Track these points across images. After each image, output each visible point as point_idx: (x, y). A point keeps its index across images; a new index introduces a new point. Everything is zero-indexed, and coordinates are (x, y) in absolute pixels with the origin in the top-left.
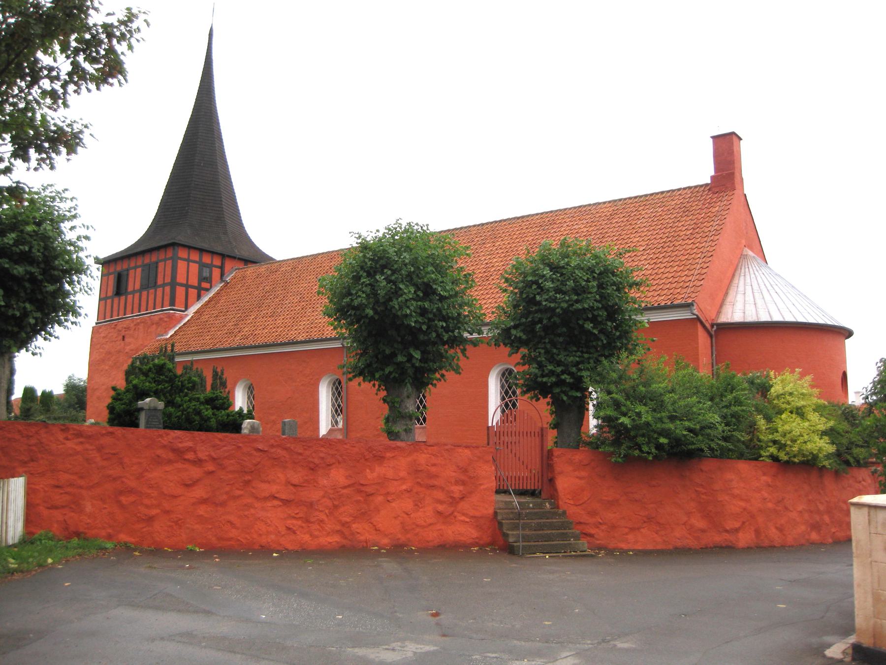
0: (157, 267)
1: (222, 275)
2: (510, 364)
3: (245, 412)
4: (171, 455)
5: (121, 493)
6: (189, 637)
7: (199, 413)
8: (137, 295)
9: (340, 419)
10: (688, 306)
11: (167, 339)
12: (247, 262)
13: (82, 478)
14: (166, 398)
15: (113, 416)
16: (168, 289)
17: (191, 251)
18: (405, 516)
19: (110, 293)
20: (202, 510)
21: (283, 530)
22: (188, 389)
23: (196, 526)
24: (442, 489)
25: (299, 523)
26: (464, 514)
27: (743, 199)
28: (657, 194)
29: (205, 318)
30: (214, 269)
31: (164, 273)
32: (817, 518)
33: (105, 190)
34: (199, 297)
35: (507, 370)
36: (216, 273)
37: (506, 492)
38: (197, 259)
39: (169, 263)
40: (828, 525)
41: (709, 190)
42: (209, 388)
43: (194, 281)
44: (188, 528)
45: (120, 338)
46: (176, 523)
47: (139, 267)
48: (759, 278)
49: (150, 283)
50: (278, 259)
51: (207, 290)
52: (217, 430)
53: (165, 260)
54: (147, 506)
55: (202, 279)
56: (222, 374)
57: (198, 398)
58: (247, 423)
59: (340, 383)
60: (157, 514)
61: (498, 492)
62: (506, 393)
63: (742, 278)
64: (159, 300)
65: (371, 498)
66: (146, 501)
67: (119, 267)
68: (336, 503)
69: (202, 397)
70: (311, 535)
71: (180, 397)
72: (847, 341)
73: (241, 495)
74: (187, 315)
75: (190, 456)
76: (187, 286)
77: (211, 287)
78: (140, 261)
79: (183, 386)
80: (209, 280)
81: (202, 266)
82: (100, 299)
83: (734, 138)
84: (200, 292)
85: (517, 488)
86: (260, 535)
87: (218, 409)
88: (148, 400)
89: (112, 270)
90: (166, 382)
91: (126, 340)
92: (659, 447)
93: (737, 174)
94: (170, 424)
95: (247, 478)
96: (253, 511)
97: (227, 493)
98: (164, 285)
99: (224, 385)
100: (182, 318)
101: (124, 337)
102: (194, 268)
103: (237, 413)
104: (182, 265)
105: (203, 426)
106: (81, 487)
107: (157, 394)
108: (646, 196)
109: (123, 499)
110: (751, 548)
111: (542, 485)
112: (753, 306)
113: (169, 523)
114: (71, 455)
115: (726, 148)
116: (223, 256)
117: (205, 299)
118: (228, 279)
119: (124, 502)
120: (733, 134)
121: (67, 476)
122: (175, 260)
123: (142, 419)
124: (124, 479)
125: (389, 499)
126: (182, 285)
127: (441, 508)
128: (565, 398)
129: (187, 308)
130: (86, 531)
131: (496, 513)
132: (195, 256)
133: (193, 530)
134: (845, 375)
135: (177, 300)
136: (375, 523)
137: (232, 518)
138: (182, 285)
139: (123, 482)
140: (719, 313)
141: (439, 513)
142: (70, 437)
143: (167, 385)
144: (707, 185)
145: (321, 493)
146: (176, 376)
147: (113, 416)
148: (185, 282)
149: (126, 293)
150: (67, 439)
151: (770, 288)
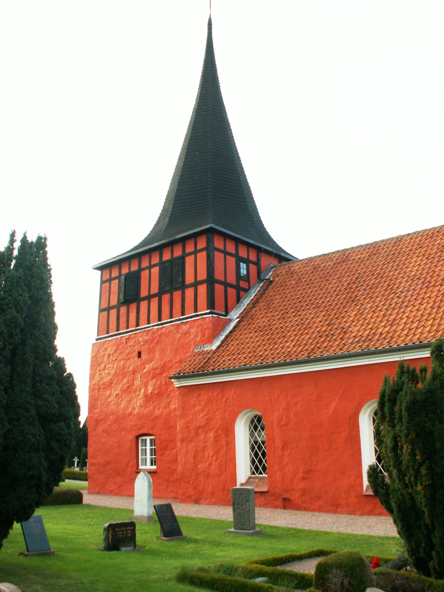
8: (154, 303)
16: (202, 290)
19: (114, 301)
34: (238, 300)
35: (255, 417)
39: (202, 257)
43: (232, 279)
45: (136, 353)
50: (300, 258)
51: (246, 291)
74: (230, 321)
76: (226, 285)
82: (101, 310)
89: (115, 273)
98: (149, 298)
102: (231, 261)
110: (57, 577)
116: (259, 250)
117: (246, 302)
126: (220, 283)
138: (220, 283)
149: (183, 286)
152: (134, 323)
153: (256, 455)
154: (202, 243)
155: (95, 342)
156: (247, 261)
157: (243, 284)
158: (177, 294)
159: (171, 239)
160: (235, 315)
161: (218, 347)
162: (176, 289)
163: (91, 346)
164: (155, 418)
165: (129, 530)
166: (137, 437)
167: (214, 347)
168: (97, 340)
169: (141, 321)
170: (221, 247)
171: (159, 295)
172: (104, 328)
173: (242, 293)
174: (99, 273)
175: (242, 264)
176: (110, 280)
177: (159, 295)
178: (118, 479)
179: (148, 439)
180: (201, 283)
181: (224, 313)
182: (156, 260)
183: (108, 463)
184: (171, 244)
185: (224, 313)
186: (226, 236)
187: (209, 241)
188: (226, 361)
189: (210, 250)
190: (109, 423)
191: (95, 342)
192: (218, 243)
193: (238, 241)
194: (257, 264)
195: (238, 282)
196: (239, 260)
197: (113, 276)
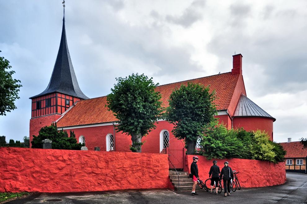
0: (51, 100)
1: (73, 103)
2: (167, 130)
3: (82, 144)
4: (53, 159)
5: (33, 173)
6: (76, 197)
7: (65, 144)
9: (112, 148)
10: (226, 110)
13: (17, 167)
14: (53, 139)
15: (33, 146)
16: (55, 107)
17: (62, 95)
18: (139, 178)
19: (35, 109)
20: (66, 178)
21: (96, 184)
22: (61, 136)
23: (64, 184)
24: (151, 168)
25: (102, 181)
26: (159, 177)
27: (242, 77)
29: (67, 116)
31: (53, 103)
32: (269, 178)
33: (33, 75)
34: (66, 110)
37: (174, 170)
39: (55, 98)
40: (272, 180)
41: (231, 74)
42: (69, 136)
43: (64, 105)
44: (61, 185)
46: (56, 183)
47: (44, 100)
48: (247, 103)
49: (49, 105)
51: (68, 108)
52: (72, 149)
53: (53, 97)
54: (44, 177)
55: (66, 104)
56: (74, 133)
57: (65, 139)
58: (82, 148)
59: (112, 136)
60: (49, 180)
61: (170, 169)
62: (165, 139)
63: (241, 102)
64: (47, 112)
65: (127, 172)
66: (44, 176)
67: (38, 100)
68: (115, 174)
69: (66, 139)
70: (107, 186)
71: (58, 139)
72: (274, 123)
73: (81, 172)
74: (62, 115)
75: (61, 158)
76: (61, 106)
78: (44, 98)
79: (59, 135)
81: (66, 100)
82: (32, 111)
83: (241, 56)
85: (177, 168)
86: (88, 186)
87: (72, 143)
88: (46, 140)
90: (53, 134)
91: (42, 124)
92: (223, 154)
93: (240, 69)
94: (54, 147)
95: (83, 166)
96: (85, 178)
97: (75, 172)
98: (53, 106)
99: (74, 136)
100: (60, 116)
102: (63, 100)
103: (79, 144)
104: (59, 100)
105: (67, 148)
106: (17, 171)
107: (49, 138)
108: (210, 76)
109: (34, 175)
111: (184, 167)
112: (245, 111)
113: (53, 183)
114: (11, 159)
115: (237, 59)
116: (73, 97)
117: (68, 110)
119: (35, 176)
120: (240, 54)
121: (10, 167)
123: (44, 145)
124: (35, 168)
125: (134, 172)
127: (151, 175)
128: (191, 139)
129: (62, 114)
130: (20, 187)
131: (169, 177)
132: (63, 96)
133: (63, 185)
134: (273, 133)
136: (129, 181)
137: (78, 180)
138: (60, 106)
139: (34, 169)
140: (234, 113)
141: (150, 177)
142: (11, 152)
143: (53, 135)
144: (230, 72)
145: (110, 171)
146: (56, 132)
147: (33, 146)
150: (10, 153)
151: (250, 105)
153: (165, 143)
158: (40, 110)
162: (40, 109)
163: (30, 120)
169: (62, 112)
170: (60, 97)
171: (46, 108)
173: (67, 108)
174: (31, 100)
175: (67, 101)
176: (34, 102)
177: (46, 108)
180: (55, 105)
194: (73, 101)
195: (66, 105)
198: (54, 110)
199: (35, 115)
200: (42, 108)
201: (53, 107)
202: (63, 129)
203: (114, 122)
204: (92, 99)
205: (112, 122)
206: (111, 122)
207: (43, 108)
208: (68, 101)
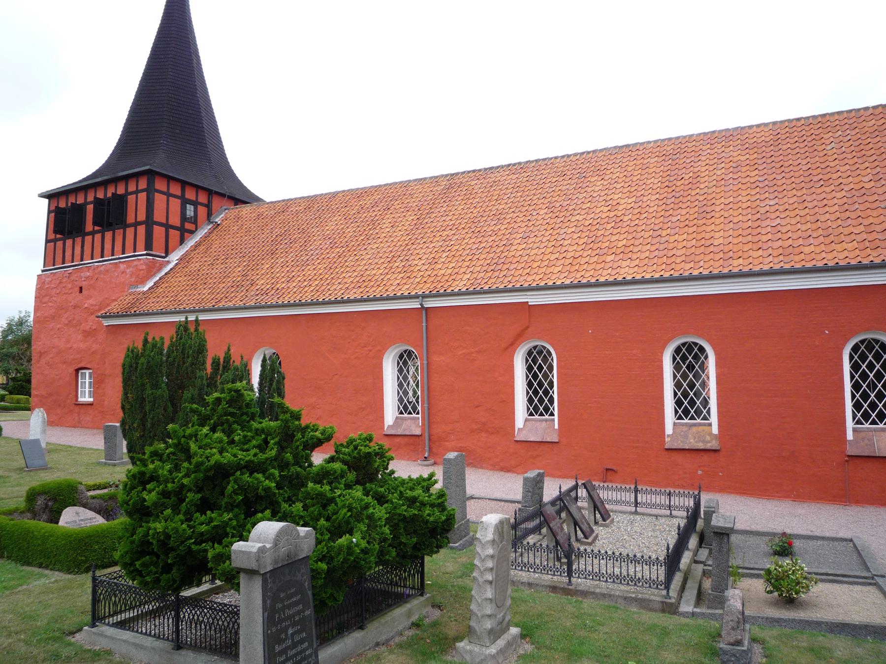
11: (144, 293)
12: (237, 201)
16: (142, 230)
28: (469, 172)
29: (194, 266)
30: (199, 207)
34: (182, 241)
35: (405, 351)
36: (202, 211)
38: (179, 193)
39: (143, 196)
43: (175, 220)
45: (78, 289)
50: (268, 201)
51: (192, 232)
55: (184, 218)
74: (168, 262)
76: (167, 226)
77: (196, 229)
80: (195, 221)
84: (184, 233)
98: (136, 224)
101: (81, 288)
102: (175, 204)
104: (160, 201)
116: (210, 192)
117: (190, 243)
118: (218, 220)
122: (150, 191)
135: (155, 244)
148: (164, 222)
152: (79, 258)
154: (143, 184)
155: (40, 273)
156: (195, 204)
157: (188, 226)
159: (113, 176)
160: (174, 257)
161: (150, 289)
164: (93, 353)
165: (678, 508)
166: (77, 371)
167: (146, 288)
168: (43, 271)
169: (105, 252)
170: (164, 189)
172: (51, 258)
178: (59, 411)
179: (87, 372)
180: (141, 223)
181: (164, 255)
182: (90, 198)
183: (50, 395)
184: (115, 181)
185: (164, 255)
186: (169, 179)
187: (150, 183)
188: (153, 305)
189: (150, 191)
190: (51, 355)
191: (40, 273)
192: (160, 185)
193: (184, 184)
195: (182, 223)
196: (185, 202)
197: (140, 188)
198: (100, 244)
199: (59, 258)
200: (129, 226)
201: (132, 229)
202: (187, 318)
203: (424, 296)
204: (272, 202)
205: (416, 297)
206: (410, 297)
207: (136, 224)
208: (192, 207)
